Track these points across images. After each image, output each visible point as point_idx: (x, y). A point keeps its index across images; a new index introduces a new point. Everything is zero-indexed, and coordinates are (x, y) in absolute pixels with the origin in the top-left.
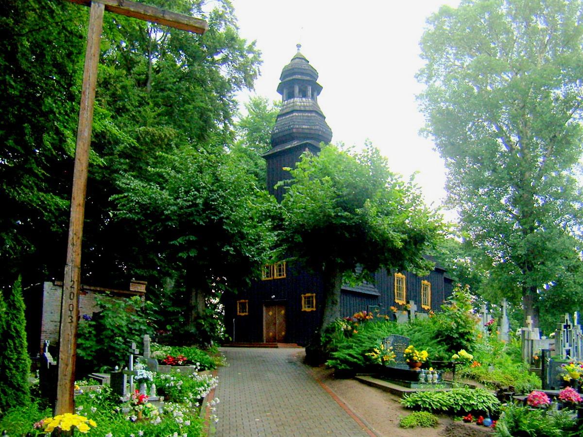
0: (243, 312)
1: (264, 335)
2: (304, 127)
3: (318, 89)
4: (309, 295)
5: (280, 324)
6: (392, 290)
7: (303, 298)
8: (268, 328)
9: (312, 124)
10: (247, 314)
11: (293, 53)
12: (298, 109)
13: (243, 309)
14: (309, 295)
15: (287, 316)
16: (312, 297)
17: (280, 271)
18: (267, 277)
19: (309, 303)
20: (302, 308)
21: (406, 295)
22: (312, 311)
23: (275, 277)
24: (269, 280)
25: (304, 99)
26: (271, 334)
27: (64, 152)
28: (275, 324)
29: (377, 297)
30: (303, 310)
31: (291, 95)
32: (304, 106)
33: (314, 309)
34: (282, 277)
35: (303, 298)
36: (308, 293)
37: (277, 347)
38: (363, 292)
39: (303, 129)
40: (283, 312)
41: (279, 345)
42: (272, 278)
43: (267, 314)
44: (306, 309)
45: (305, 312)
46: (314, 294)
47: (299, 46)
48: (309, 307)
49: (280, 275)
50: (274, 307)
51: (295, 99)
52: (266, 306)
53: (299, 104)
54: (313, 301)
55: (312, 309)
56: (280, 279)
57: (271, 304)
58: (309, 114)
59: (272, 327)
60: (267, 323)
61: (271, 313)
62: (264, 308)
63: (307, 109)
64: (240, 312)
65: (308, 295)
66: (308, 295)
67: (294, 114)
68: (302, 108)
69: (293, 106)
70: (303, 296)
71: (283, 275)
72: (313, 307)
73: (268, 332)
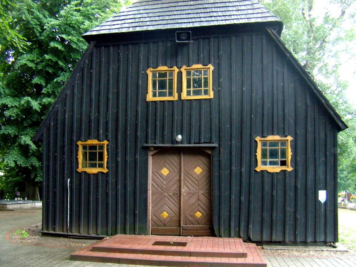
4: (95, 142)
5: (190, 195)
16: (284, 143)
20: (257, 165)
23: (184, 96)
26: (165, 214)
30: (258, 169)
33: (289, 169)
43: (160, 173)
55: (284, 168)
65: (90, 142)
71: (206, 92)
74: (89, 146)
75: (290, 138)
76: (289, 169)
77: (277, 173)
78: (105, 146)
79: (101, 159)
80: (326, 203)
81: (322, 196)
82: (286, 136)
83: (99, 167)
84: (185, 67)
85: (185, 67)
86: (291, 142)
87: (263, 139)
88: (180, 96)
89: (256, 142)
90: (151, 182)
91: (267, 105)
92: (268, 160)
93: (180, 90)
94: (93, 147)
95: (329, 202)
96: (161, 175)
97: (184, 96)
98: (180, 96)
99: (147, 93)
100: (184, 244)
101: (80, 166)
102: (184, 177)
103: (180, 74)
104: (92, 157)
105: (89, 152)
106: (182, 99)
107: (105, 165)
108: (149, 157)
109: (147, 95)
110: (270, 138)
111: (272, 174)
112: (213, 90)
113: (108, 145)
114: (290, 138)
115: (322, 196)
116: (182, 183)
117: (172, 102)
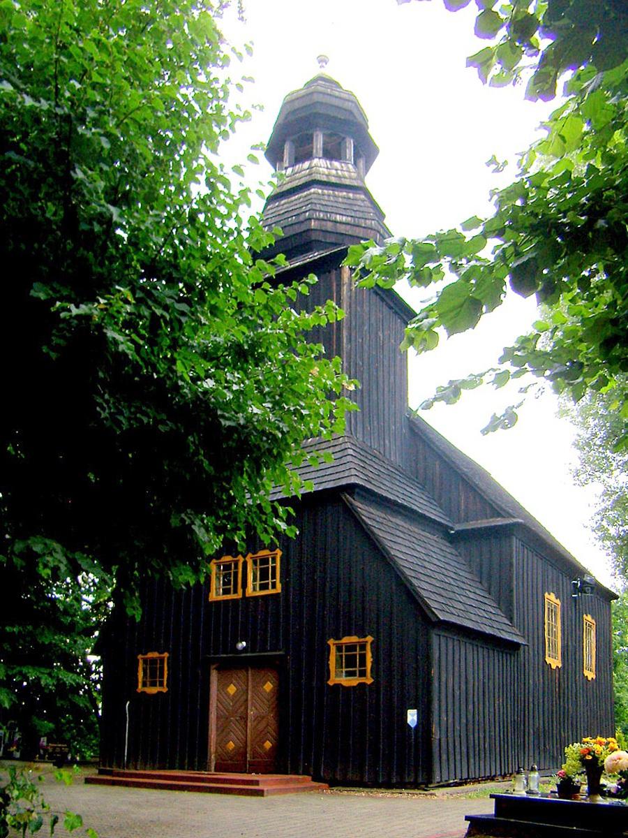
0: (153, 684)
1: (212, 747)
2: (338, 218)
3: (366, 151)
4: (155, 655)
5: (259, 719)
6: (540, 632)
7: (333, 649)
8: (222, 729)
9: (360, 215)
10: (165, 690)
11: (313, 71)
12: (325, 179)
13: (153, 678)
14: (155, 655)
15: (281, 698)
16: (363, 647)
17: (264, 575)
18: (226, 592)
19: (351, 662)
20: (329, 678)
21: (563, 647)
22: (362, 685)
23: (250, 591)
24: (233, 600)
25: (336, 164)
26: (231, 745)
27: (42, 757)
28: (244, 718)
29: (516, 646)
30: (331, 683)
31: (303, 155)
32: (337, 176)
33: (369, 680)
34: (270, 591)
35: (333, 649)
36: (152, 650)
37: (260, 793)
38: (488, 630)
39: (336, 222)
40: (268, 687)
41: (265, 781)
42: (239, 595)
43: (223, 692)
44: (339, 678)
45: (338, 686)
46: (166, 655)
47: (323, 60)
48: (349, 674)
49: (226, 592)
50: (242, 674)
51: (316, 161)
52: (218, 669)
53: (326, 172)
54: (363, 657)
55: (362, 680)
56: (263, 597)
57: (232, 665)
58: (351, 195)
59: (236, 728)
60: (218, 718)
61: (232, 689)
62: (214, 676)
63: (347, 182)
64: (144, 685)
65: (152, 655)
66: (152, 655)
67: (312, 190)
68: (333, 180)
69: (310, 174)
70: (331, 642)
71: (274, 586)
72: (363, 674)
73: (222, 743)
74: (346, 647)
75: (369, 639)
76: (369, 680)
77: (354, 687)
78: (166, 659)
79: (363, 663)
80: (416, 727)
81: (412, 717)
82: (365, 636)
83: (360, 676)
84: (250, 555)
85: (250, 555)
86: (372, 643)
87: (337, 642)
88: (244, 592)
89: (329, 646)
90: (215, 705)
91: (343, 596)
92: (344, 670)
93: (245, 585)
94: (351, 647)
95: (420, 726)
96: (227, 694)
97: (250, 591)
98: (244, 592)
99: (210, 591)
100: (257, 783)
101: (333, 674)
102: (252, 697)
103: (245, 564)
104: (350, 662)
105: (346, 655)
106: (247, 595)
107: (165, 683)
108: (212, 671)
109: (210, 594)
110: (346, 640)
111: (348, 688)
112: (281, 582)
113: (168, 658)
114: (369, 639)
115: (412, 717)
116: (250, 703)
117: (237, 600)
